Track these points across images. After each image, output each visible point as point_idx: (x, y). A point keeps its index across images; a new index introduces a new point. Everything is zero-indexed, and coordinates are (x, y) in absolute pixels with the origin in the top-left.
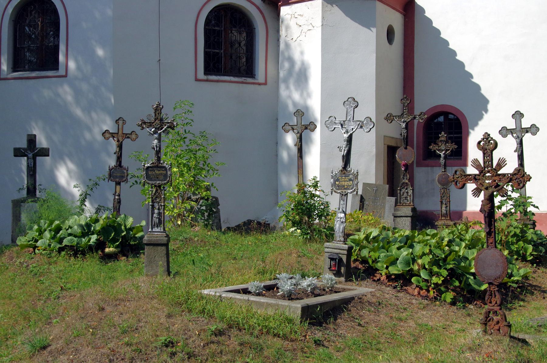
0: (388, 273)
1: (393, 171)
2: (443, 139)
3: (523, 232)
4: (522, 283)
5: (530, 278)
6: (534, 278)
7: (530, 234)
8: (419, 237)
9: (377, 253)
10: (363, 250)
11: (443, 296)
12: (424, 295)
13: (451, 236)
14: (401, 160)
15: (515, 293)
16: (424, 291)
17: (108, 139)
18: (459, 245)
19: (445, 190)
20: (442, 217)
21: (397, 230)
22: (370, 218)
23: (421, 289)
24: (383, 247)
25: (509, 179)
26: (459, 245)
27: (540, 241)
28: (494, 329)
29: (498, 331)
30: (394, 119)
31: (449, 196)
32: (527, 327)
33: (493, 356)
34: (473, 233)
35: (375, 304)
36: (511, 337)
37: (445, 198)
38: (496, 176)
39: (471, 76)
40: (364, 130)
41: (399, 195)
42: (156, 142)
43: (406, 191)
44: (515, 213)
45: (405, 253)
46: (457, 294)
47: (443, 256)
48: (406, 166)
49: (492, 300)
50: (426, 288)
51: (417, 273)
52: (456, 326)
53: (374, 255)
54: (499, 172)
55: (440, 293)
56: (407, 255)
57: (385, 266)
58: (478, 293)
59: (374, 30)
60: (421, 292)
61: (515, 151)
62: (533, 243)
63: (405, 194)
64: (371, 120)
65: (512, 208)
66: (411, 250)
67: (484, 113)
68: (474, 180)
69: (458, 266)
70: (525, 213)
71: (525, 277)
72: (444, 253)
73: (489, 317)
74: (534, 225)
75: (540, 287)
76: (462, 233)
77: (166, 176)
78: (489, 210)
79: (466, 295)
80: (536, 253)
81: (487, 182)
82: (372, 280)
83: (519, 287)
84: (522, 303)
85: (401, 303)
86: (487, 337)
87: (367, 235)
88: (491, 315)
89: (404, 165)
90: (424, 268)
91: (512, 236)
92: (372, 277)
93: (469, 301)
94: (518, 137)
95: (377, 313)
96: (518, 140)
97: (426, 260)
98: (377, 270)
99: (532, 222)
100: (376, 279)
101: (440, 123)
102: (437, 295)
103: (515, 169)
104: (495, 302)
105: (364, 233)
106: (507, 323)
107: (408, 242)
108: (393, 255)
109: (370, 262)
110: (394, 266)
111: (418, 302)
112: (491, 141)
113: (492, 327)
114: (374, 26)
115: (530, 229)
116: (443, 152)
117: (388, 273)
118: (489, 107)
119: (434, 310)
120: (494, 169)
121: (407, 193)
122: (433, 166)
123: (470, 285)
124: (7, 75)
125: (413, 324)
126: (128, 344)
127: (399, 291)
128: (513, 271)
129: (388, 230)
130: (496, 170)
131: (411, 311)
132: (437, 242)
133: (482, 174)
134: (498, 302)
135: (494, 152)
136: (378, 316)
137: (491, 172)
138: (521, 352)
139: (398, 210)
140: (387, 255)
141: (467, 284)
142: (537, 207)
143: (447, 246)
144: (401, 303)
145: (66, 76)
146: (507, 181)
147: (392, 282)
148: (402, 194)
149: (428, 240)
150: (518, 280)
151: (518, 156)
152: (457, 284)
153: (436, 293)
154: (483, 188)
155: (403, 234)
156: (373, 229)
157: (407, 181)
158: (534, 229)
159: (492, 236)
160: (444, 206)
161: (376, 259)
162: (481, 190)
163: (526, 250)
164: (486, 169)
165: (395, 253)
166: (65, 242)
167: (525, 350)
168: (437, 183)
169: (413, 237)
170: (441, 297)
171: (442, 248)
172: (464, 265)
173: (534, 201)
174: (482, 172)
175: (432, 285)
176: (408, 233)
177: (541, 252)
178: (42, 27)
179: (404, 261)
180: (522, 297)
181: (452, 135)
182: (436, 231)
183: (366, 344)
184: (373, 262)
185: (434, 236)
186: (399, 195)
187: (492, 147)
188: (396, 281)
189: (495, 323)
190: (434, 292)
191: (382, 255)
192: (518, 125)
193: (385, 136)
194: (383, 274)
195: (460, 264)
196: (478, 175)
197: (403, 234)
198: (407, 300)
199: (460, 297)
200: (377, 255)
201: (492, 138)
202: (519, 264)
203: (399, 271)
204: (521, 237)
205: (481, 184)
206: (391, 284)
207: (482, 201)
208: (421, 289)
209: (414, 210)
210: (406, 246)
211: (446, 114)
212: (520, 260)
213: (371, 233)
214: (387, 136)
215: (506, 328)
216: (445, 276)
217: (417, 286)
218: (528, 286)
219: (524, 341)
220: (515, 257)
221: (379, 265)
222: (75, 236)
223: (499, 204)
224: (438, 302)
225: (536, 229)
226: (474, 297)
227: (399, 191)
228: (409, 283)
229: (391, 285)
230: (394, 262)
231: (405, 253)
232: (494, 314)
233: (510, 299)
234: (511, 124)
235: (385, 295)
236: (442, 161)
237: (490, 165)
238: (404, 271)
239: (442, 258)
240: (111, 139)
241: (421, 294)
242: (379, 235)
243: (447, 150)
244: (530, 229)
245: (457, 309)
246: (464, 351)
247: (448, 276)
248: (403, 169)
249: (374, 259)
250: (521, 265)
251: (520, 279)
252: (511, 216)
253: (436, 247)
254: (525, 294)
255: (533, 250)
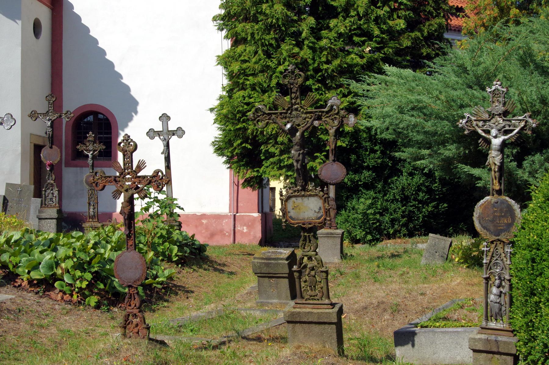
0: (29, 278)
1: (40, 170)
2: (90, 139)
3: (169, 233)
4: (167, 284)
5: (175, 279)
6: (179, 278)
7: (176, 235)
8: (63, 240)
9: (18, 257)
10: (4, 254)
11: (87, 300)
12: (68, 300)
13: (97, 238)
14: (46, 160)
15: (160, 294)
16: (68, 295)
18: (105, 248)
19: (93, 191)
20: (89, 219)
21: (41, 233)
22: (14, 220)
23: (65, 293)
24: (25, 251)
25: (148, 181)
26: (105, 248)
27: (186, 242)
28: (133, 332)
29: (137, 334)
30: (38, 116)
31: (97, 198)
32: (168, 328)
33: (131, 360)
34: (119, 234)
35: (14, 311)
36: (150, 339)
37: (93, 201)
38: (135, 178)
39: (120, 76)
40: (4, 127)
41: (44, 196)
43: (52, 192)
44: (162, 214)
45: (48, 257)
46: (102, 298)
47: (88, 259)
48: (51, 166)
49: (132, 303)
50: (70, 292)
51: (60, 277)
52: (100, 331)
53: (14, 260)
54: (139, 175)
55: (85, 297)
56: (50, 259)
57: (27, 271)
58: (122, 295)
59: (19, 22)
60: (65, 297)
61: (162, 153)
62: (178, 244)
63: (50, 196)
64: (12, 116)
65: (159, 210)
66: (54, 254)
67: (133, 114)
68: (114, 182)
69: (103, 268)
70: (171, 214)
71: (170, 278)
72: (89, 256)
73: (128, 320)
74: (180, 226)
75: (184, 287)
76: (110, 235)
78: (129, 212)
79: (110, 298)
80: (181, 254)
81: (127, 183)
82: (12, 286)
83: (163, 288)
84: (166, 304)
85: (43, 310)
86: (127, 340)
87: (8, 238)
88: (130, 318)
89: (49, 165)
90: (68, 272)
91: (159, 238)
92: (12, 283)
93: (113, 304)
94: (165, 139)
95: (17, 320)
96: (165, 143)
97: (69, 264)
98: (18, 275)
99: (177, 223)
100: (17, 285)
101: (89, 123)
102: (81, 299)
103: (154, 172)
104: (134, 304)
105: (5, 236)
106: (145, 325)
107: (52, 245)
108: (36, 259)
109: (11, 266)
110: (37, 270)
111: (61, 307)
112: (131, 143)
113: (131, 330)
114: (19, 19)
115: (176, 230)
116: (91, 153)
117: (29, 278)
118: (139, 108)
119: (78, 315)
120: (134, 171)
121: (53, 194)
122: (82, 167)
123: (115, 287)
125: (55, 331)
127: (41, 297)
128: (158, 272)
129: (32, 233)
130: (136, 172)
131: (53, 317)
132: (82, 244)
133: (122, 176)
134: (138, 305)
135: (134, 154)
136: (18, 324)
137: (131, 174)
138: (159, 353)
139: (43, 212)
140: (29, 259)
141: (112, 287)
142: (182, 209)
143: (92, 248)
144: (43, 310)
146: (147, 183)
147: (34, 288)
148: (47, 195)
149: (72, 243)
150: (163, 281)
151: (165, 158)
152: (102, 286)
153: (80, 297)
154: (123, 190)
155: (47, 237)
156: (14, 233)
157: (52, 182)
158: (180, 230)
159: (132, 239)
160: (92, 207)
161: (17, 264)
162: (121, 193)
163: (171, 251)
164: (126, 171)
165: (38, 257)
167: (163, 351)
168: (85, 184)
169: (58, 240)
170: (85, 301)
171: (87, 250)
172: (109, 267)
173: (179, 202)
174: (122, 174)
175: (77, 290)
176: (52, 235)
177: (186, 252)
179: (47, 265)
180: (166, 298)
181: (102, 136)
182: (81, 234)
183: (4, 354)
184: (14, 267)
185: (78, 239)
186: (44, 196)
187: (132, 149)
188: (39, 286)
189: (134, 325)
190: (78, 297)
191: (24, 259)
192: (165, 128)
193: (31, 134)
194: (25, 279)
195: (105, 267)
196: (119, 177)
197: (47, 237)
198: (49, 306)
199: (105, 300)
200: (17, 259)
201: (132, 140)
202: (164, 265)
203: (42, 276)
204: (167, 238)
205: (121, 186)
206: (32, 289)
207: (122, 204)
208: (65, 293)
209: (60, 212)
210: (50, 249)
211: (95, 114)
212: (166, 261)
213: (12, 236)
214: (34, 135)
215: (145, 331)
216: (89, 280)
217: (60, 291)
218: (173, 287)
219: (162, 343)
220: (161, 258)
221: (20, 270)
223: (146, 205)
224: (82, 307)
225: (182, 230)
226: (118, 300)
227: (43, 193)
228: (52, 287)
229: (33, 291)
230: (36, 267)
231: (48, 256)
232: (133, 317)
233: (154, 300)
234: (158, 127)
235: (27, 301)
236: (90, 161)
237: (130, 167)
238: (47, 276)
239: (86, 261)
241: (65, 299)
242: (20, 239)
243: (94, 151)
244: (176, 230)
245: (101, 312)
246: (103, 356)
247: (92, 279)
248: (48, 169)
249: (15, 264)
250: (167, 266)
251: (165, 280)
252: (157, 217)
253: (80, 251)
254: (169, 295)
255: (178, 251)
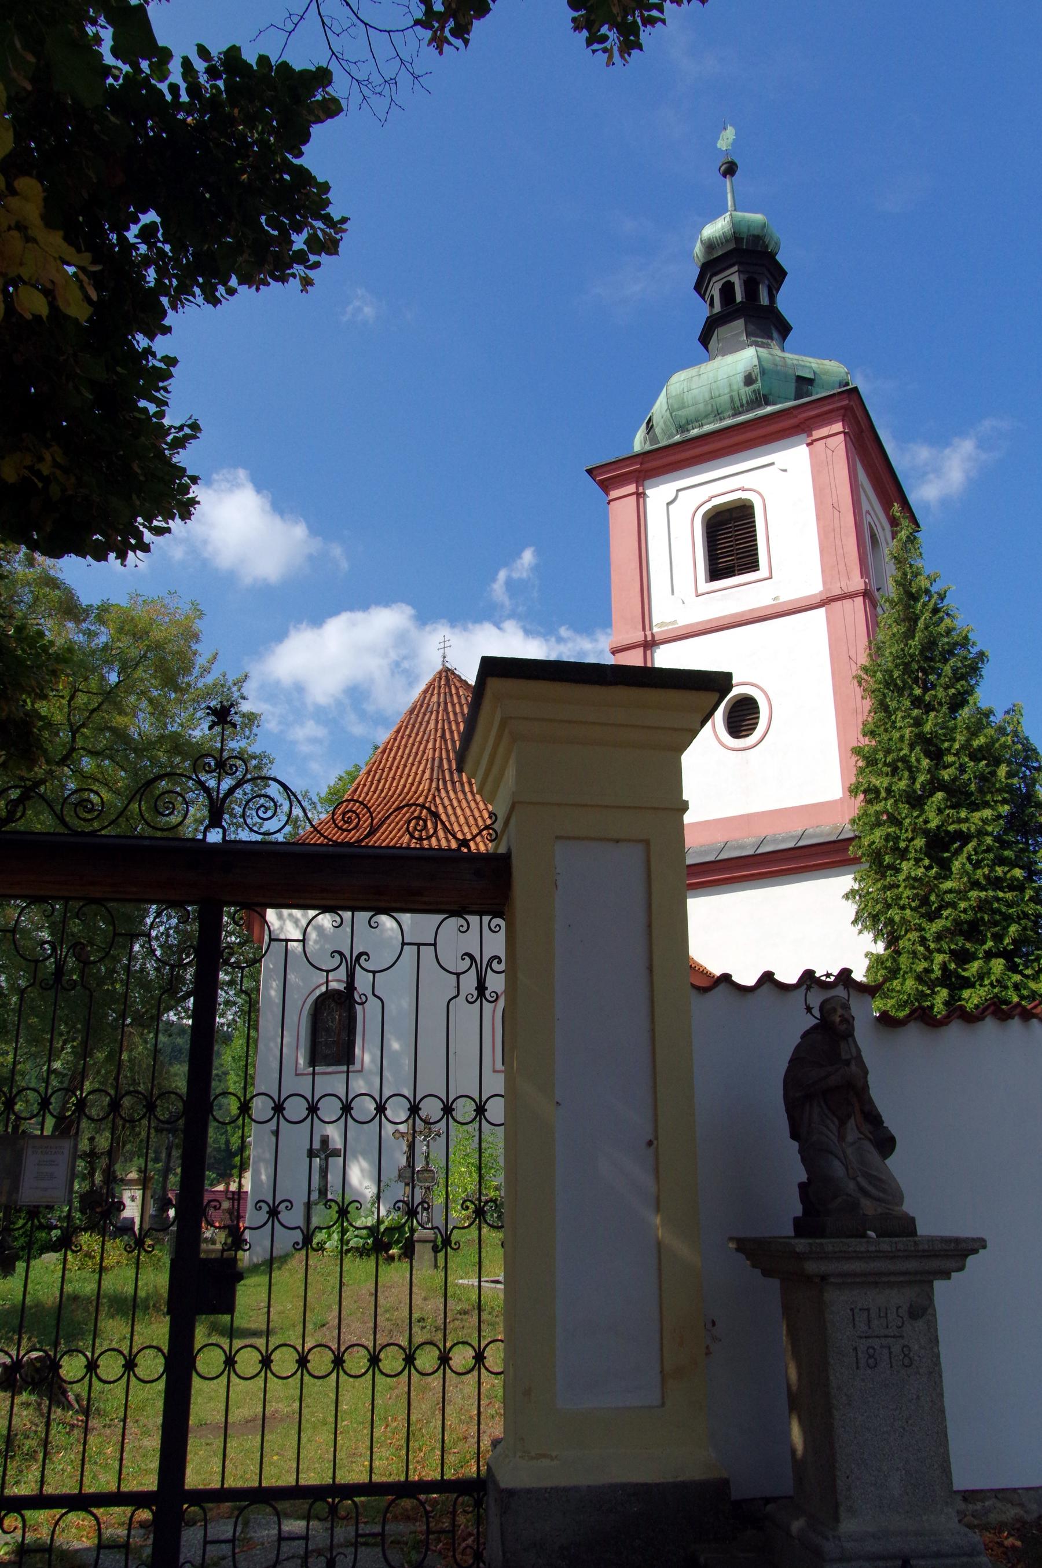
17: (398, 1138)
42: (425, 1148)
77: (433, 1178)
124: (304, 1069)
126: (388, 1320)
145: (361, 1071)
166: (352, 1244)
178: (340, 1020)
222: (361, 1238)
240: (401, 1138)
